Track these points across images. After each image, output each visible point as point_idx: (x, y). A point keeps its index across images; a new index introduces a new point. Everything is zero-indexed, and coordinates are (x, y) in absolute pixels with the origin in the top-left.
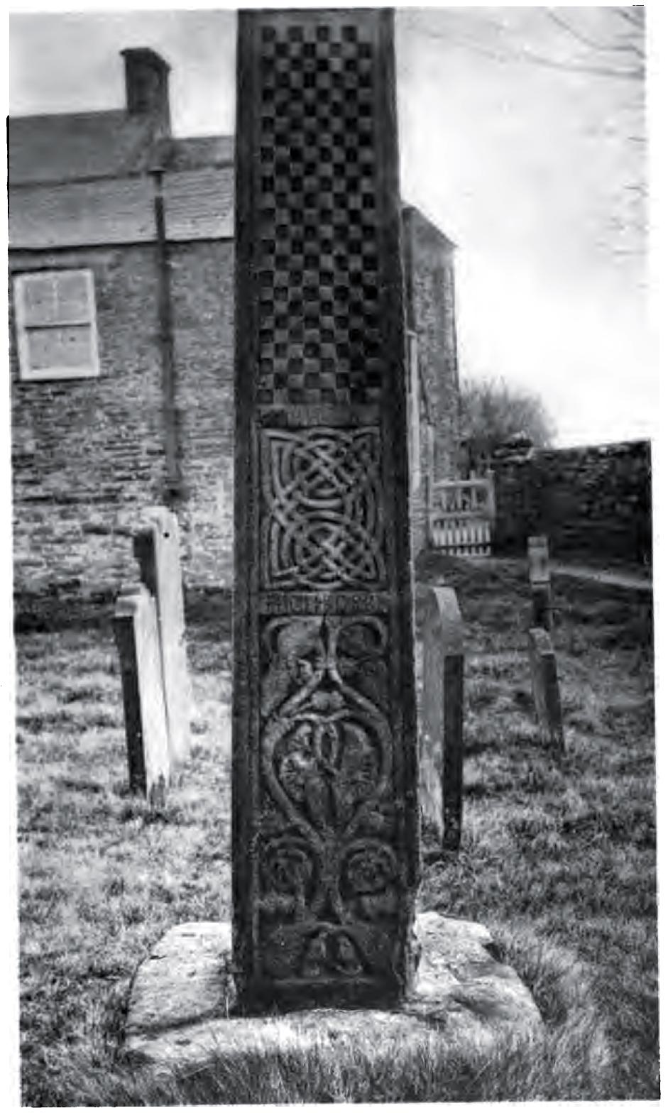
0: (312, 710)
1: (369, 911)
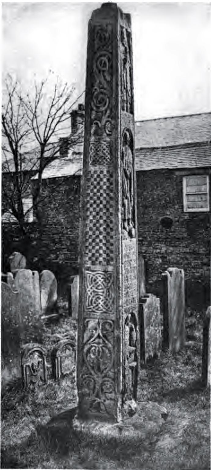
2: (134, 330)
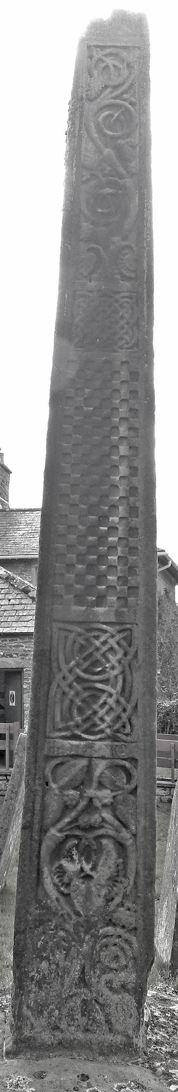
0: (78, 827)
1: (123, 775)
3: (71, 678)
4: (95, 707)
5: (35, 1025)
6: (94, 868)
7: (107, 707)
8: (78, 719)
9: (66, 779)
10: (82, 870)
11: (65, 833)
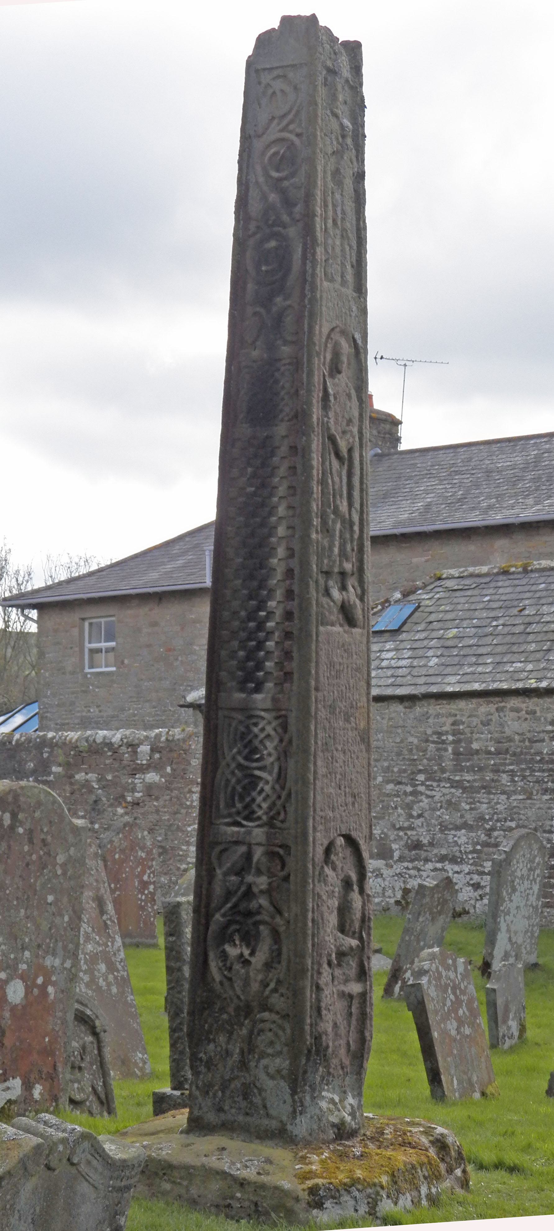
0: (239, 913)
1: (278, 861)
2: (355, 887)
3: (233, 765)
4: (254, 794)
5: (203, 1105)
6: (252, 954)
7: (263, 795)
8: (239, 806)
9: (229, 865)
10: (242, 955)
11: (228, 918)
